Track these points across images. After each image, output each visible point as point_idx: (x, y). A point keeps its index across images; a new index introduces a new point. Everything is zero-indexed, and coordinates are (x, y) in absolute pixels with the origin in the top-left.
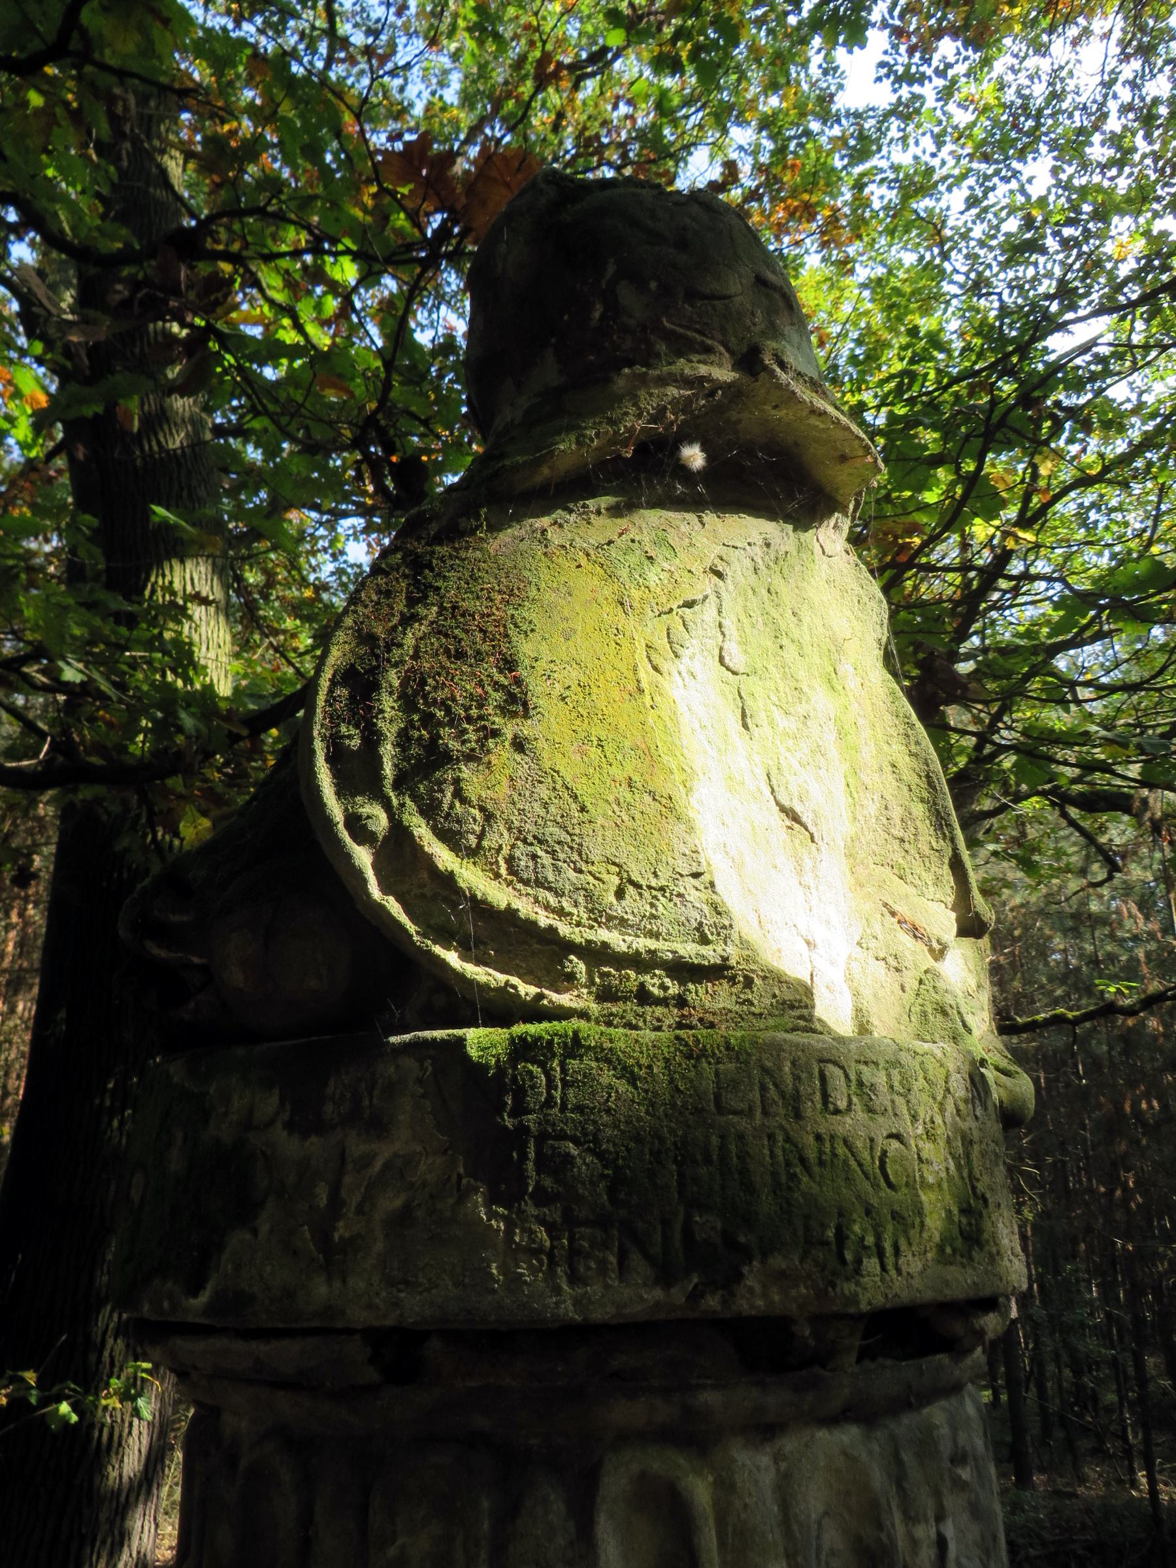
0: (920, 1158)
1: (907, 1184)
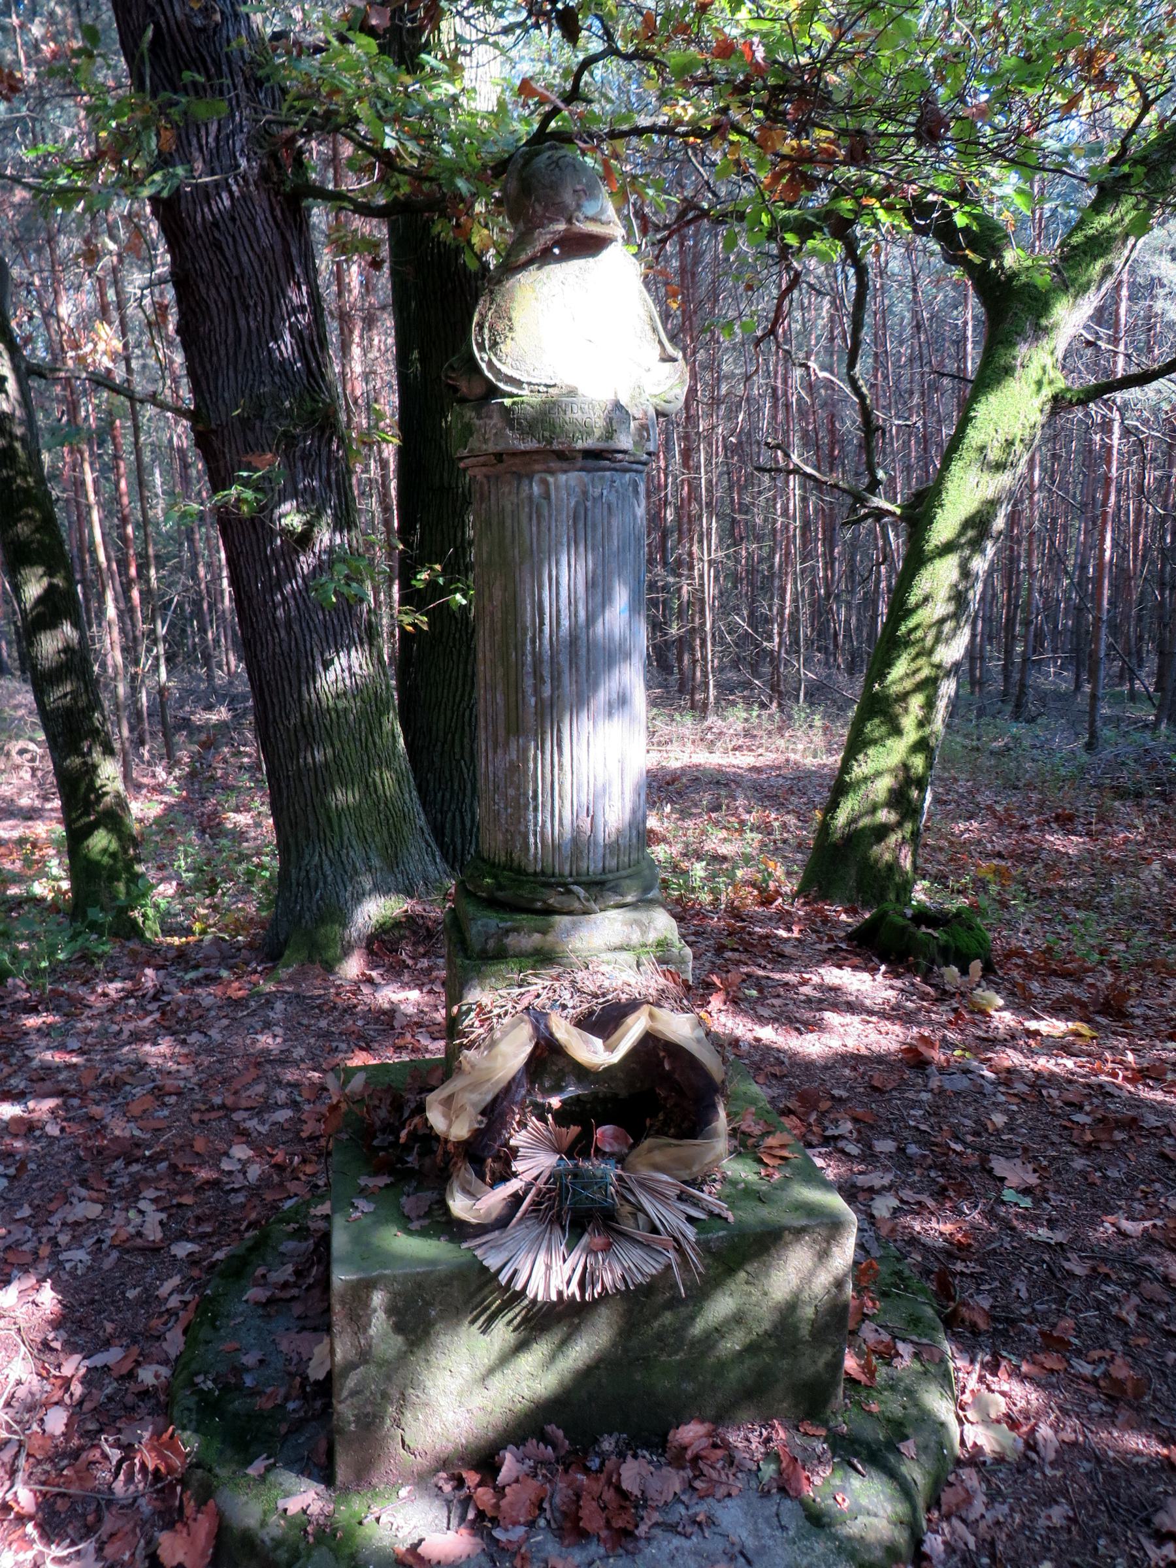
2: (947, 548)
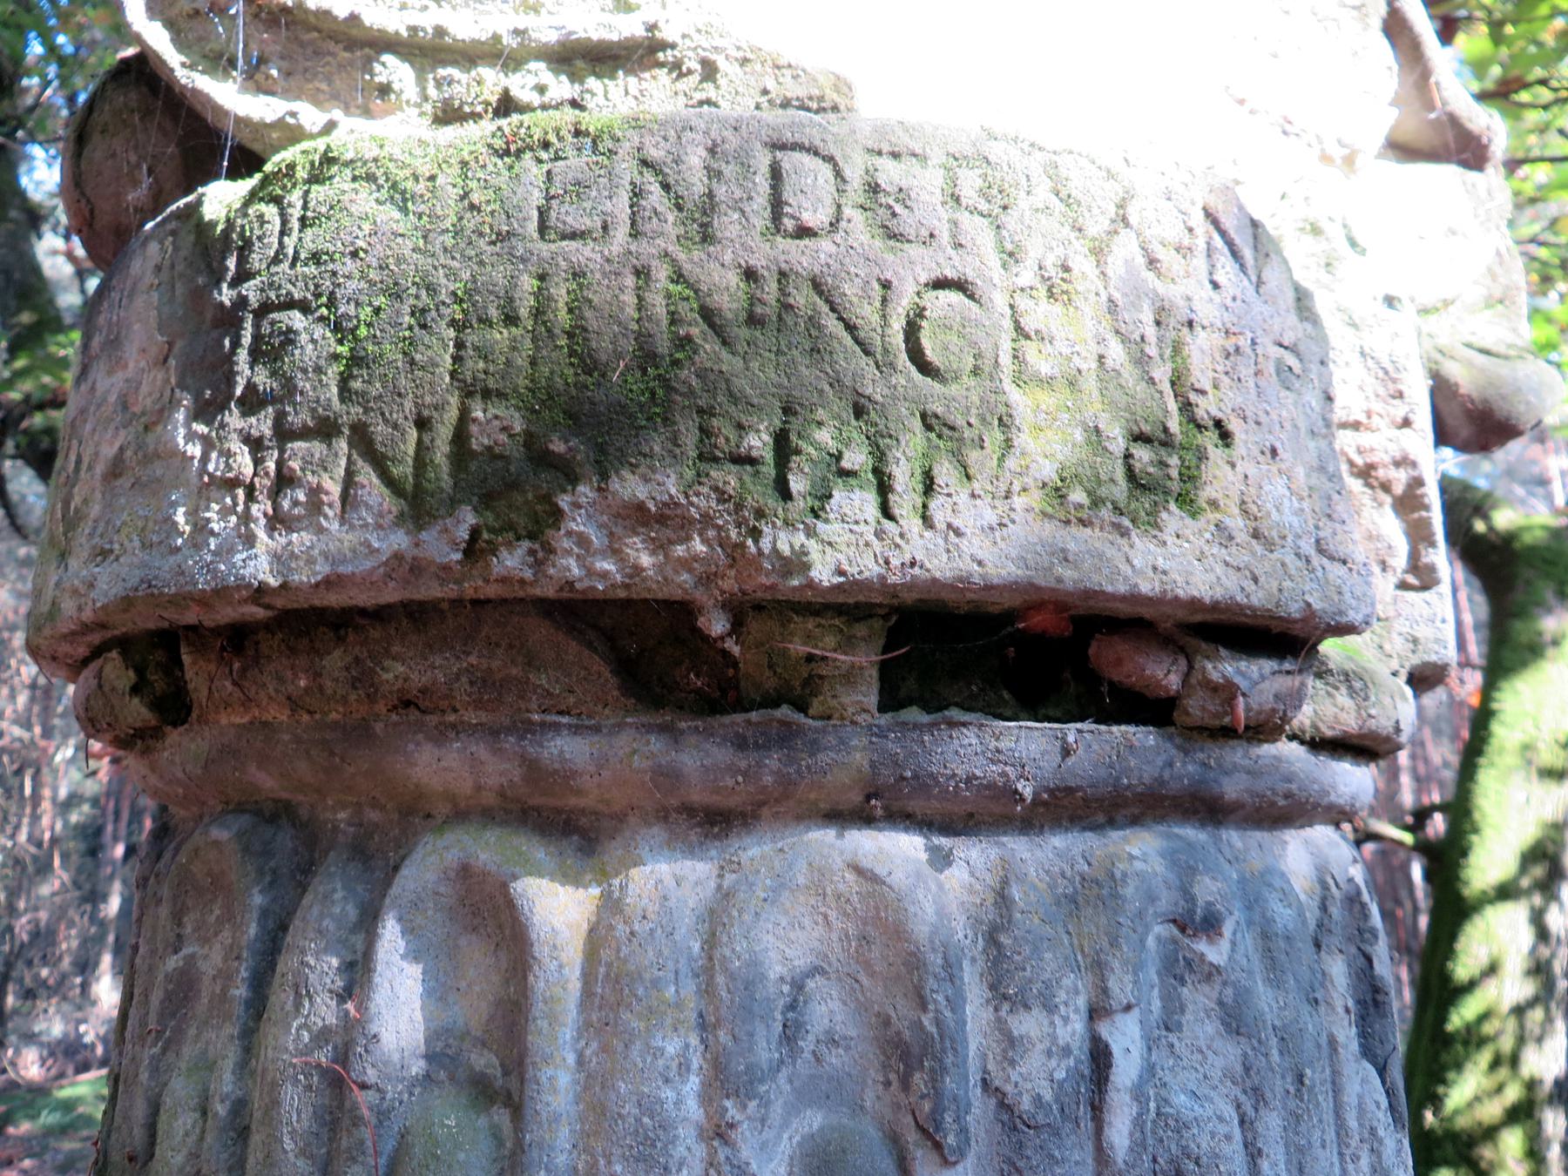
0: (1018, 328)
1: (976, 371)
2: (1505, 892)
